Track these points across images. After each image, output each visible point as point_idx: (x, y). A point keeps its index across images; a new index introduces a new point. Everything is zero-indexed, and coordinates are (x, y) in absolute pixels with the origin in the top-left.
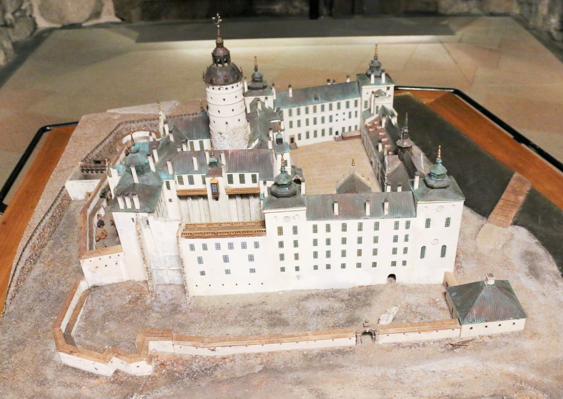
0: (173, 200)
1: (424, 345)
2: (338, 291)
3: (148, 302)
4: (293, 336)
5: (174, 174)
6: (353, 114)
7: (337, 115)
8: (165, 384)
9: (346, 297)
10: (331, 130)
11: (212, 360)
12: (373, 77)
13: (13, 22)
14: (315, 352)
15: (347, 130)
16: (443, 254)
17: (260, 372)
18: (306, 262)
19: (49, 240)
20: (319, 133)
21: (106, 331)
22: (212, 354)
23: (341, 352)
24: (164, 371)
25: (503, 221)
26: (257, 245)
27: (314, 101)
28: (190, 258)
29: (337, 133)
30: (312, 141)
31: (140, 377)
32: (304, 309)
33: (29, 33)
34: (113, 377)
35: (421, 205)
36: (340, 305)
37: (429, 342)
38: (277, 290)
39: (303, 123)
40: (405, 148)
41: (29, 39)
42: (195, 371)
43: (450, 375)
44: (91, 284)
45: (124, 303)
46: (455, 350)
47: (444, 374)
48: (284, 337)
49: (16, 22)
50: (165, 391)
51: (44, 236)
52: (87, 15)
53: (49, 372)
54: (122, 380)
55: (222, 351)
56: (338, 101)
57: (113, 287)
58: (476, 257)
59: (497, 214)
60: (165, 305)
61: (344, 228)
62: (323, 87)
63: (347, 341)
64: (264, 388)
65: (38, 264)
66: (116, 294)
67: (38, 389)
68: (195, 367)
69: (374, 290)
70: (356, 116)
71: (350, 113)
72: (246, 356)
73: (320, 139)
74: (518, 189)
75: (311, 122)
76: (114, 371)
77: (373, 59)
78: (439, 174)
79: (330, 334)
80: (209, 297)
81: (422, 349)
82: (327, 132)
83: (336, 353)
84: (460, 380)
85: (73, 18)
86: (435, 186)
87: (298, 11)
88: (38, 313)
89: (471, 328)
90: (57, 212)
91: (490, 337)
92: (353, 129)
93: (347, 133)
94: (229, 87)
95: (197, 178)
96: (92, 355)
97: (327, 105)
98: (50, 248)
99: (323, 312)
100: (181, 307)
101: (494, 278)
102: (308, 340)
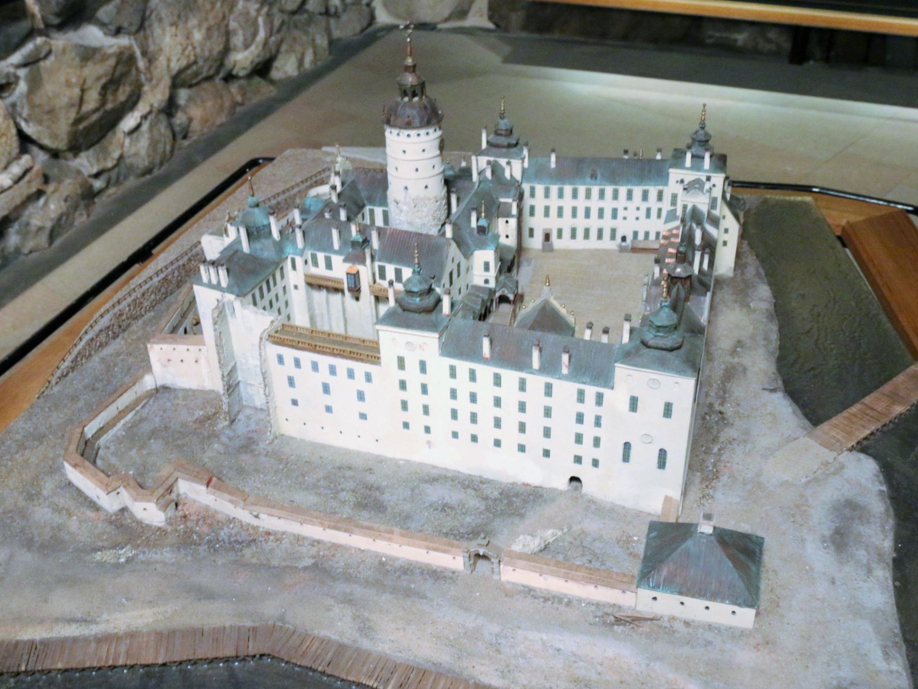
0: (299, 287)
1: (569, 603)
2: (489, 482)
3: (220, 426)
4: (371, 528)
5: (304, 248)
6: (654, 213)
7: (626, 209)
8: (172, 546)
9: (496, 494)
10: (613, 232)
11: (251, 531)
12: (689, 156)
13: (340, 10)
14: (397, 564)
15: (641, 237)
16: (662, 464)
17: (306, 568)
18: (440, 422)
19: (149, 311)
20: (593, 234)
21: (145, 452)
22: (255, 522)
23: (436, 575)
24: (182, 526)
25: (838, 441)
26: (368, 378)
27: (589, 180)
28: (279, 375)
29: (624, 239)
30: (580, 243)
31: (148, 526)
32: (421, 495)
33: (358, 29)
34: (116, 515)
35: (621, 371)
36: (478, 505)
37: (580, 600)
38: (398, 456)
39: (567, 212)
40: (676, 278)
41: (356, 38)
42: (220, 539)
43: (581, 664)
44: (159, 383)
45: (190, 419)
46: (616, 627)
47: (573, 659)
48: (357, 526)
49: (344, 10)
50: (167, 555)
51: (141, 303)
52: (446, 13)
53: (48, 486)
54: (124, 522)
55: (269, 522)
56: (630, 187)
57: (189, 394)
58: (749, 487)
59: (836, 426)
60: (238, 437)
61: (497, 380)
62: (609, 160)
63: (453, 561)
64: (296, 593)
65: (118, 340)
66: (185, 405)
67: (22, 503)
68: (223, 534)
69: (541, 496)
70: (659, 216)
71: (648, 210)
72: (299, 539)
73: (593, 243)
74: (902, 394)
75: (581, 213)
76: (120, 507)
77: (697, 127)
78: (659, 324)
79: (426, 540)
80: (302, 441)
81: (562, 608)
82: (607, 234)
83: (428, 573)
84: (594, 677)
85: (426, 16)
86: (651, 343)
87: (773, 47)
88: (81, 404)
89: (655, 598)
90: (176, 274)
91: (687, 624)
92: (652, 237)
93: (640, 241)
94: (413, 133)
95: (337, 260)
96: (97, 475)
97: (609, 190)
98: (144, 322)
99: (445, 508)
100: (257, 445)
101: (712, 523)
102: (390, 540)
